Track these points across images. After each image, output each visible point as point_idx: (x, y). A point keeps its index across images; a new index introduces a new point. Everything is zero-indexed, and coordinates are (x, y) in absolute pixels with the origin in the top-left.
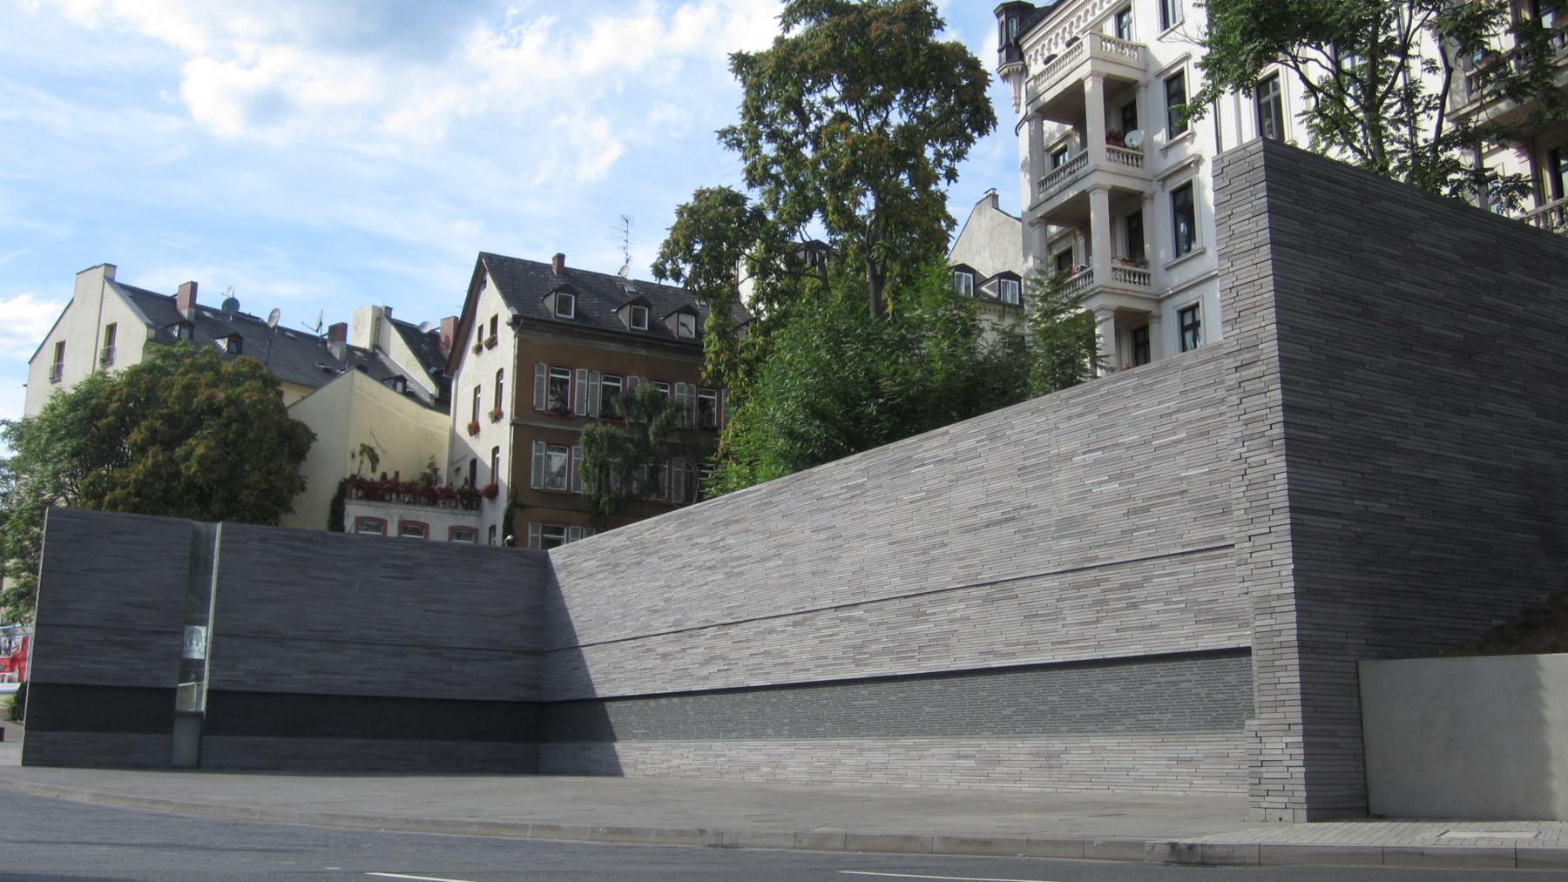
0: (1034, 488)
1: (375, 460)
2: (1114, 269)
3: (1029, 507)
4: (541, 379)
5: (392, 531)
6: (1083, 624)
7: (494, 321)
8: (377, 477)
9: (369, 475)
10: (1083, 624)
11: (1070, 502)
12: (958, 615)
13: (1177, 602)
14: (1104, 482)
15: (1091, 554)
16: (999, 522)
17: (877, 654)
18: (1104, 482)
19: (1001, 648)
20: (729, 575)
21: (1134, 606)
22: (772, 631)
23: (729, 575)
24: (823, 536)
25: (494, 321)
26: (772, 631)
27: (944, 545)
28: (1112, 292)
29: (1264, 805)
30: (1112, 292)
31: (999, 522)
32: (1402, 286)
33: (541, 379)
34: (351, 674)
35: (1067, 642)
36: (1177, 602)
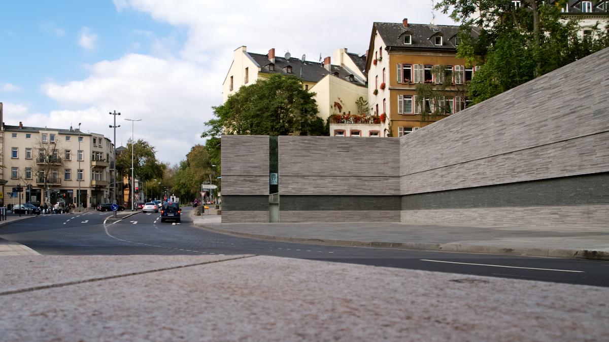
0: (584, 98)
1: (340, 108)
5: (348, 134)
7: (381, 48)
12: (552, 155)
17: (520, 172)
19: (569, 168)
22: (480, 165)
24: (498, 125)
25: (381, 48)
26: (480, 165)
27: (545, 125)
34: (330, 187)
35: (597, 164)
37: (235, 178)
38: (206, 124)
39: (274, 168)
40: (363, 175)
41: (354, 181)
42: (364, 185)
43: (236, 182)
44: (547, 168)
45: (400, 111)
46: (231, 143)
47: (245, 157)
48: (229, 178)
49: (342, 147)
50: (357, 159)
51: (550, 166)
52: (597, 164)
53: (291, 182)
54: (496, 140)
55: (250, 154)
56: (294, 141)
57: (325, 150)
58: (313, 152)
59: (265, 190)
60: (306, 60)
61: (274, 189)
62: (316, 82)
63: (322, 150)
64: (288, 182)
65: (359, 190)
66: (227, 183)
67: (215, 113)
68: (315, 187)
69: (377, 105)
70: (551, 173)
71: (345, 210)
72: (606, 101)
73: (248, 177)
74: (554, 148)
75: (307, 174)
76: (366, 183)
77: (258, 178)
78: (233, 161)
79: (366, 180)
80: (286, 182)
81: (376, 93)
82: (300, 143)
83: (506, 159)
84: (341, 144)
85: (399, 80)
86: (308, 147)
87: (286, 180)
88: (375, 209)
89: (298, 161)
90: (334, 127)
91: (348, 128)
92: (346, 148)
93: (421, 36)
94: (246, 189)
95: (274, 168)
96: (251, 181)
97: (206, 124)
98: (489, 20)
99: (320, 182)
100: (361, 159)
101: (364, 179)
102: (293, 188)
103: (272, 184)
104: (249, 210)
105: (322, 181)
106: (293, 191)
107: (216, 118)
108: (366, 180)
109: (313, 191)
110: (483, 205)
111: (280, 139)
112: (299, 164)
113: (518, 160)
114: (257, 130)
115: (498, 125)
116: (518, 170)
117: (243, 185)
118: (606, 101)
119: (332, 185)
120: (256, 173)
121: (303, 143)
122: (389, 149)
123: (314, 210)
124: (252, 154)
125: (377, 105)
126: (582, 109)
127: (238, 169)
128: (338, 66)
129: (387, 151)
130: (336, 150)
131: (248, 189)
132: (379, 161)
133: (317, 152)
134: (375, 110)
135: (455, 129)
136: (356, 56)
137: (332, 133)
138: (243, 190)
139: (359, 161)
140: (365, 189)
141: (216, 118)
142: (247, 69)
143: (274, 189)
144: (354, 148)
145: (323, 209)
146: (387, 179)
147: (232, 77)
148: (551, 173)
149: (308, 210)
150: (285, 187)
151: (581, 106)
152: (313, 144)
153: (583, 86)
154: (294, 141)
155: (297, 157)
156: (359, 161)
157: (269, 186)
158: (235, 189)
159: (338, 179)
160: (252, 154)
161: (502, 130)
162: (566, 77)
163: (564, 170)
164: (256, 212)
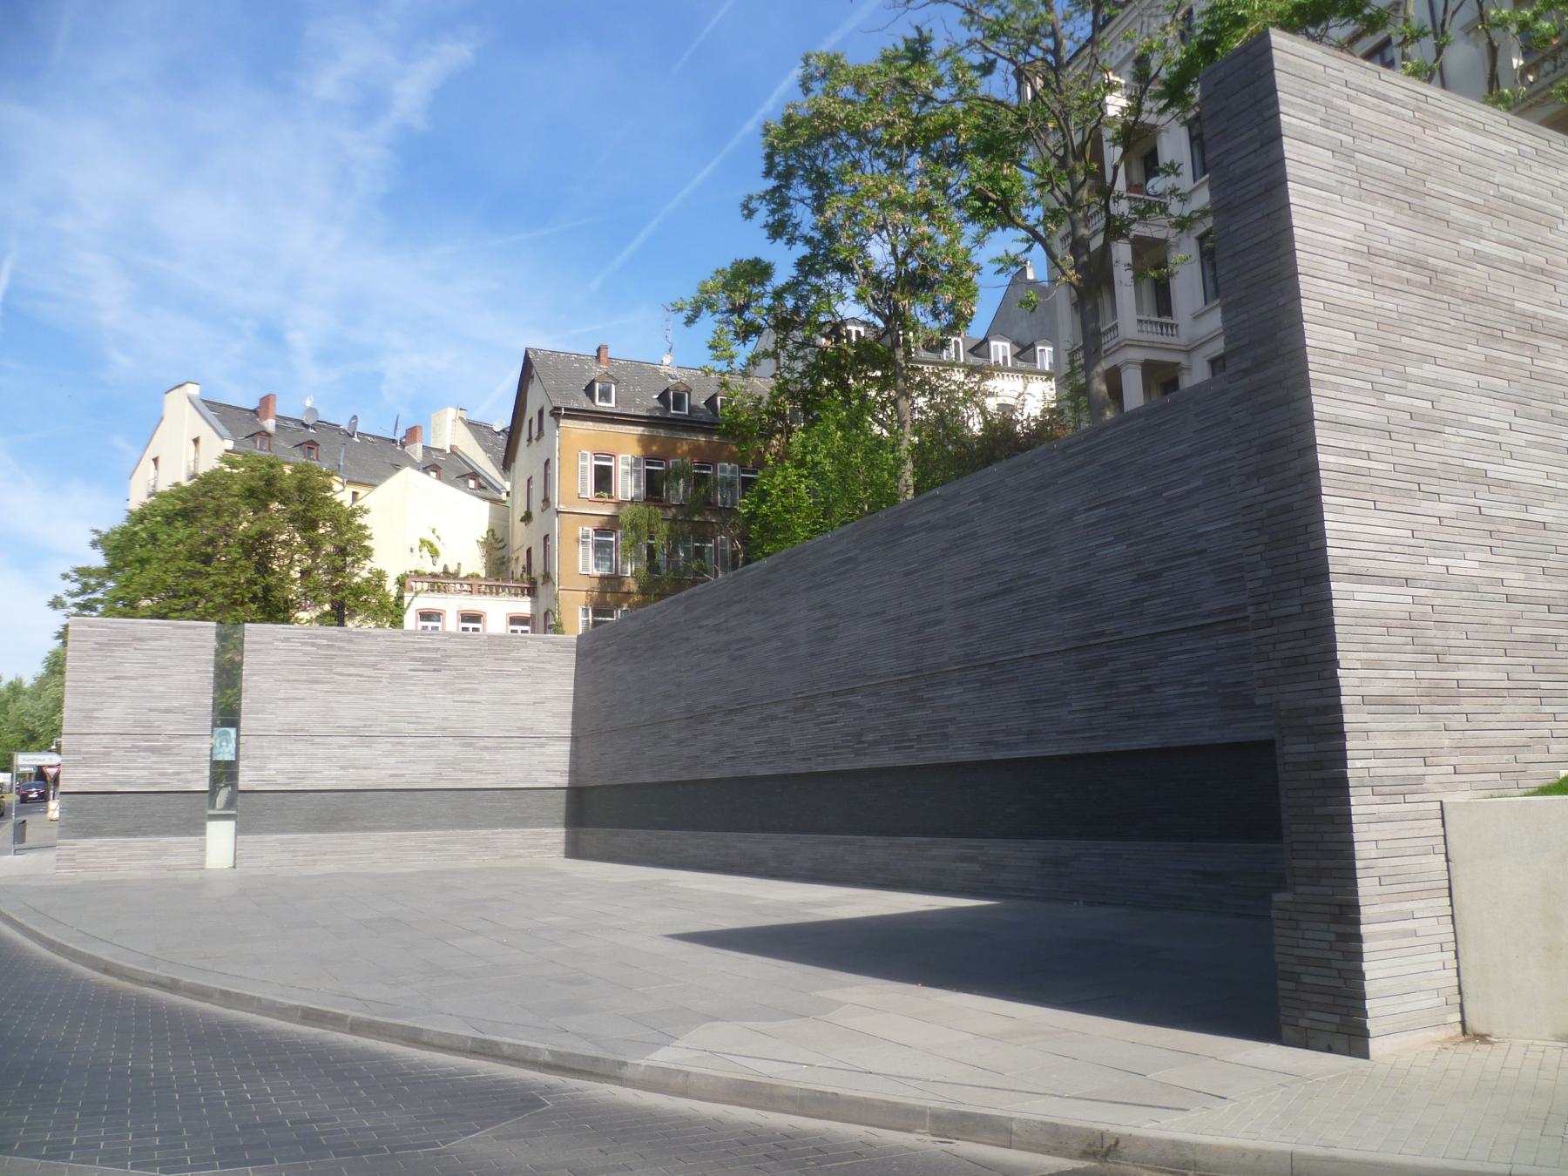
0: (1032, 554)
1: (435, 554)
2: (1140, 321)
3: (1028, 576)
4: (584, 467)
5: (452, 623)
6: (1091, 710)
7: (541, 413)
8: (438, 569)
9: (427, 566)
10: (1091, 710)
11: (1071, 569)
12: (957, 700)
13: (1198, 685)
14: (1110, 543)
15: (1098, 628)
16: (996, 595)
17: (876, 743)
18: (1110, 543)
19: (1001, 738)
20: (733, 659)
21: (1148, 689)
22: (773, 718)
23: (733, 659)
24: (818, 614)
25: (541, 413)
26: (773, 718)
27: (938, 622)
28: (1138, 345)
29: (1303, 1023)
30: (1138, 345)
31: (996, 595)
32: (1485, 247)
33: (584, 467)
34: (382, 767)
35: (1074, 732)
36: (1198, 685)
37: (106, 740)
38: (65, 576)
39: (227, 715)
40: (478, 733)
41: (451, 750)
42: (479, 761)
43: (108, 754)
44: (946, 736)
45: (585, 567)
46: (100, 639)
47: (140, 682)
48: (87, 740)
49: (421, 659)
50: (462, 691)
51: (951, 729)
52: (1074, 732)
53: (274, 752)
54: (812, 655)
55: (156, 671)
56: (287, 640)
57: (374, 666)
58: (339, 670)
59: (196, 776)
60: (361, 428)
61: (224, 772)
62: (374, 486)
63: (365, 665)
64: (266, 752)
65: (466, 776)
66: (78, 757)
67: (94, 544)
68: (342, 768)
69: (529, 551)
70: (955, 749)
71: (429, 829)
72: (1087, 564)
73: (146, 739)
74: (960, 684)
75: (321, 730)
76: (486, 755)
77: (176, 742)
78: (101, 694)
79: (486, 748)
80: (258, 753)
81: (527, 518)
82: (303, 644)
83: (841, 705)
84: (421, 650)
85: (584, 490)
86: (327, 657)
87: (261, 747)
88: (508, 826)
89: (300, 693)
90: (418, 602)
91: (451, 605)
92: (434, 662)
93: (638, 389)
94: (137, 773)
95: (227, 715)
96: (153, 750)
97: (65, 576)
98: (792, 358)
99: (361, 753)
100: (474, 691)
101: (481, 743)
102: (280, 772)
103: (220, 758)
104: (145, 834)
105: (365, 751)
106: (281, 779)
107: (98, 560)
108: (486, 748)
109: (337, 778)
110: (782, 829)
111: (256, 633)
112: (301, 703)
113: (869, 711)
114: (178, 602)
115: (818, 614)
116: (870, 737)
117: (130, 761)
118: (1087, 564)
119: (391, 760)
120: (170, 729)
121: (313, 645)
122: (547, 666)
123: (337, 831)
124: (163, 672)
125: (529, 551)
126: (1028, 584)
127: (115, 714)
128: (442, 451)
129: (544, 670)
130: (405, 667)
131: (145, 773)
132: (521, 698)
133: (352, 670)
134: (523, 561)
135: (710, 622)
136: (488, 428)
137: (410, 620)
138: (129, 776)
139: (468, 697)
140: (480, 772)
141: (98, 560)
142: (196, 441)
143: (224, 772)
144: (454, 662)
145: (365, 829)
146: (542, 746)
147: (155, 460)
148: (955, 749)
149: (321, 831)
150: (256, 769)
151: (1028, 576)
152: (340, 649)
153: (1029, 523)
154: (287, 640)
155: (297, 685)
156: (468, 697)
157: (208, 765)
158: (105, 775)
159: (411, 745)
160: (163, 672)
161: (829, 628)
162: (985, 499)
163: (989, 743)
164: (165, 840)
